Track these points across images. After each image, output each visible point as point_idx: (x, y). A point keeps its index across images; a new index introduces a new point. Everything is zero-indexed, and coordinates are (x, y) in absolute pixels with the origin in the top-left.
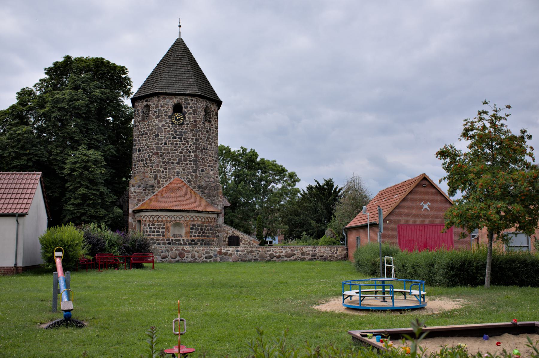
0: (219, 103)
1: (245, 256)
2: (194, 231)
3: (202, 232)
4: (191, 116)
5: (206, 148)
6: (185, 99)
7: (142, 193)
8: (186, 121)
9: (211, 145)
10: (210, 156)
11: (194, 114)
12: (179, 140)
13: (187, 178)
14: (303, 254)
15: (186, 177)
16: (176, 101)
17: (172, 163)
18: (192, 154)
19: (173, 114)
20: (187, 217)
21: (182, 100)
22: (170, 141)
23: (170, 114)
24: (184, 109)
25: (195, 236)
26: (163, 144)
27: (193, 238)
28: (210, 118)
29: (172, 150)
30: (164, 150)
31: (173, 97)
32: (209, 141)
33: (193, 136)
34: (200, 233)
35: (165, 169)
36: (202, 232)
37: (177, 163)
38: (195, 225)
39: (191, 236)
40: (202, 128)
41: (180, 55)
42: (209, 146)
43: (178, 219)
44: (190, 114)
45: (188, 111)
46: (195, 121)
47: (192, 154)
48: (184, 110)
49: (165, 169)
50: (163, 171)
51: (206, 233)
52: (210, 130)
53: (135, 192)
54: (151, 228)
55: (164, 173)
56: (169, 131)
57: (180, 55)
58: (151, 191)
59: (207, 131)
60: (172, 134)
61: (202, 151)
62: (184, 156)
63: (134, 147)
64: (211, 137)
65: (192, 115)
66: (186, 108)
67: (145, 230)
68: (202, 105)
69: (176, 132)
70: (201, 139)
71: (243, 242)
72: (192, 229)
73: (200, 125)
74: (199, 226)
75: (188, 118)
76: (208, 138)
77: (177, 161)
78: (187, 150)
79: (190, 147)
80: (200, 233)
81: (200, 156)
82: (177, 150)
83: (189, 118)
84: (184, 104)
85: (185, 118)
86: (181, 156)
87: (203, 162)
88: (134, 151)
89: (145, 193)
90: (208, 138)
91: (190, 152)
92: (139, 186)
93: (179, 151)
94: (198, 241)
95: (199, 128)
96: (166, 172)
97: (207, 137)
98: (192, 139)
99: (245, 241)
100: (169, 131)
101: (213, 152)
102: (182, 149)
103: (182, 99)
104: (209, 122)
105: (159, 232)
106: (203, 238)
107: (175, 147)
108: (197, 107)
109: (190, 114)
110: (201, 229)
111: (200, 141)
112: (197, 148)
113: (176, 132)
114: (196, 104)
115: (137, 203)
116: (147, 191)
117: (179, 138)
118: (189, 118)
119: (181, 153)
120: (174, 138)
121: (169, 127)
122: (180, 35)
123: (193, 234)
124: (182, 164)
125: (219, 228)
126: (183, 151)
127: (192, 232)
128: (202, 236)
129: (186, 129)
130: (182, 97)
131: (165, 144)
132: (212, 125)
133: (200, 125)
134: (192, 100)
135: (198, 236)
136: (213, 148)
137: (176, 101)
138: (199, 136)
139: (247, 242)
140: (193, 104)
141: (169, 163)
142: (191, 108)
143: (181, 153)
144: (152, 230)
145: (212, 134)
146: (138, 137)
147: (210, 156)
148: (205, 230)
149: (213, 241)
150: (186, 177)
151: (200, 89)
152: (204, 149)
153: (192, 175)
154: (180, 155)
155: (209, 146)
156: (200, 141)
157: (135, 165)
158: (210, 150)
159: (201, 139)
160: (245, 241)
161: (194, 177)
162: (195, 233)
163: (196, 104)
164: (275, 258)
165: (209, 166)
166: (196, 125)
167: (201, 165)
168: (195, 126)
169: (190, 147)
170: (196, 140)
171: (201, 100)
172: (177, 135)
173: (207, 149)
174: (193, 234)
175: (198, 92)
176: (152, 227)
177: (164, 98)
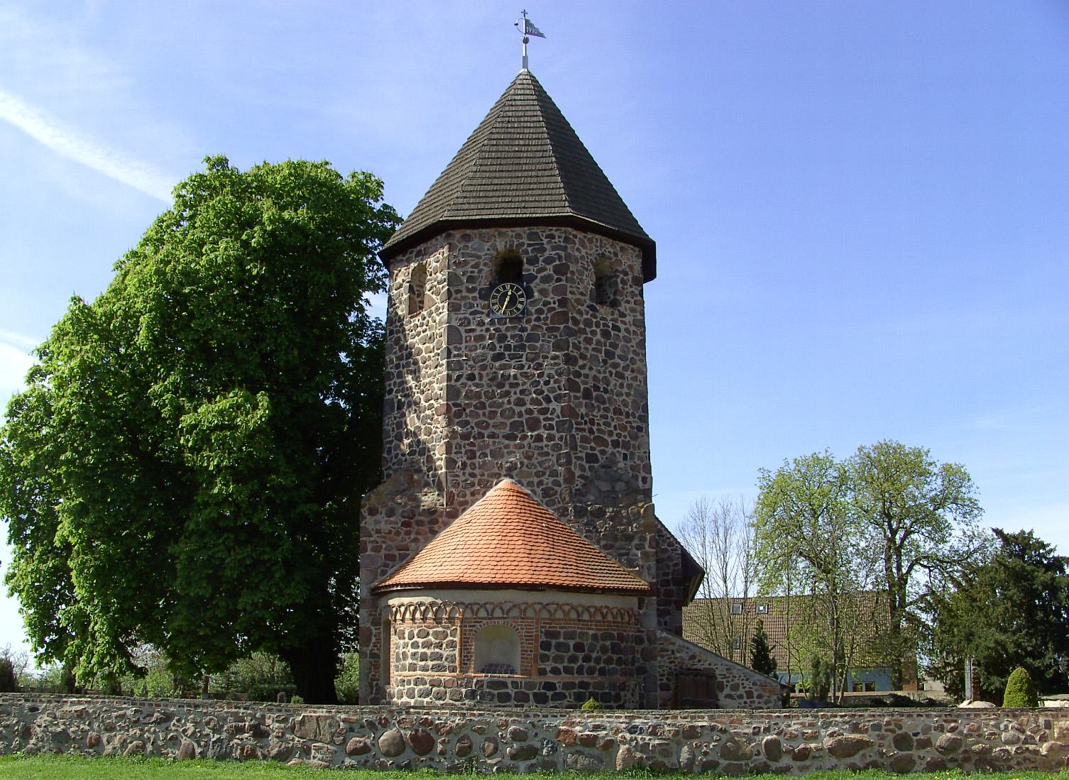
0: (647, 250)
1: (664, 750)
2: (552, 653)
3: (581, 655)
4: (549, 287)
5: (602, 386)
6: (530, 236)
7: (398, 534)
8: (533, 303)
9: (620, 376)
10: (618, 411)
11: (558, 280)
12: (513, 363)
13: (540, 483)
14: (902, 741)
15: (536, 480)
16: (500, 243)
17: (492, 436)
18: (553, 405)
19: (492, 286)
20: (559, 606)
21: (519, 239)
22: (484, 368)
23: (483, 283)
24: (526, 266)
25: (555, 671)
26: (463, 380)
27: (550, 678)
28: (615, 294)
29: (490, 396)
30: (467, 397)
31: (491, 231)
32: (615, 366)
33: (557, 347)
34: (573, 659)
35: (472, 455)
36: (581, 655)
37: (507, 437)
38: (555, 635)
39: (542, 672)
40: (588, 323)
41: (534, 132)
42: (613, 381)
43: (498, 613)
44: (546, 279)
45: (539, 271)
46: (563, 302)
47: (553, 405)
48: (528, 269)
49: (472, 455)
50: (464, 465)
51: (598, 660)
52: (616, 328)
53: (378, 531)
54: (415, 645)
55: (468, 470)
56: (481, 338)
57: (534, 132)
58: (425, 528)
59: (606, 334)
60: (492, 347)
61: (587, 394)
62: (530, 412)
63: (387, 397)
64: (618, 352)
65: (554, 284)
66: (533, 261)
67: (401, 651)
68: (586, 249)
69: (502, 338)
70: (583, 357)
71: (727, 691)
72: (546, 646)
73: (580, 312)
74: (570, 636)
75: (541, 292)
76: (610, 355)
77: (507, 431)
78: (540, 392)
79: (547, 383)
80: (573, 659)
81: (583, 410)
82: (507, 394)
83: (542, 292)
84: (526, 252)
85: (529, 294)
86: (520, 415)
87: (591, 431)
88: (387, 409)
89: (408, 533)
90: (610, 355)
91: (548, 400)
92: (391, 513)
93: (513, 398)
94: (567, 686)
95: (576, 322)
96: (473, 466)
97: (607, 352)
98: (555, 358)
99: (735, 688)
100: (481, 338)
101: (629, 400)
102: (522, 392)
103: (519, 236)
104: (614, 304)
105: (440, 657)
106: (586, 678)
107: (501, 386)
108: (568, 257)
109: (546, 279)
110: (579, 647)
111: (581, 362)
112: (572, 386)
113: (502, 338)
114: (565, 249)
115: (386, 565)
116: (415, 528)
117: (512, 357)
118: (543, 294)
119: (520, 402)
120: (498, 357)
121: (481, 323)
122: (525, 65)
123: (548, 666)
124: (525, 437)
125: (646, 644)
126: (528, 399)
127: (544, 658)
128: (580, 670)
129: (535, 328)
130: (518, 230)
131: (471, 377)
132: (622, 315)
133: (580, 312)
134: (551, 237)
135: (568, 670)
136: (630, 386)
137: (500, 243)
138: (576, 347)
139: (741, 691)
140: (553, 248)
141: (481, 435)
142: (548, 261)
143: (520, 402)
144: (421, 650)
145: (621, 344)
146: (397, 366)
147: (618, 411)
148: (592, 649)
149: (623, 687)
150: (536, 480)
151: (574, 201)
152: (597, 388)
153: (554, 474)
154: (517, 409)
155: (613, 381)
156: (581, 362)
157: (389, 452)
158: (619, 394)
159: (583, 357)
160: (735, 688)
161: (561, 479)
162: (556, 659)
163: (565, 249)
164: (786, 761)
165: (616, 444)
166: (565, 314)
167: (584, 439)
168: (564, 317)
169: (547, 383)
170: (569, 360)
171: (580, 235)
172: (508, 348)
173: (606, 391)
174: (548, 666)
175: (568, 212)
176: (421, 641)
177: (466, 238)
